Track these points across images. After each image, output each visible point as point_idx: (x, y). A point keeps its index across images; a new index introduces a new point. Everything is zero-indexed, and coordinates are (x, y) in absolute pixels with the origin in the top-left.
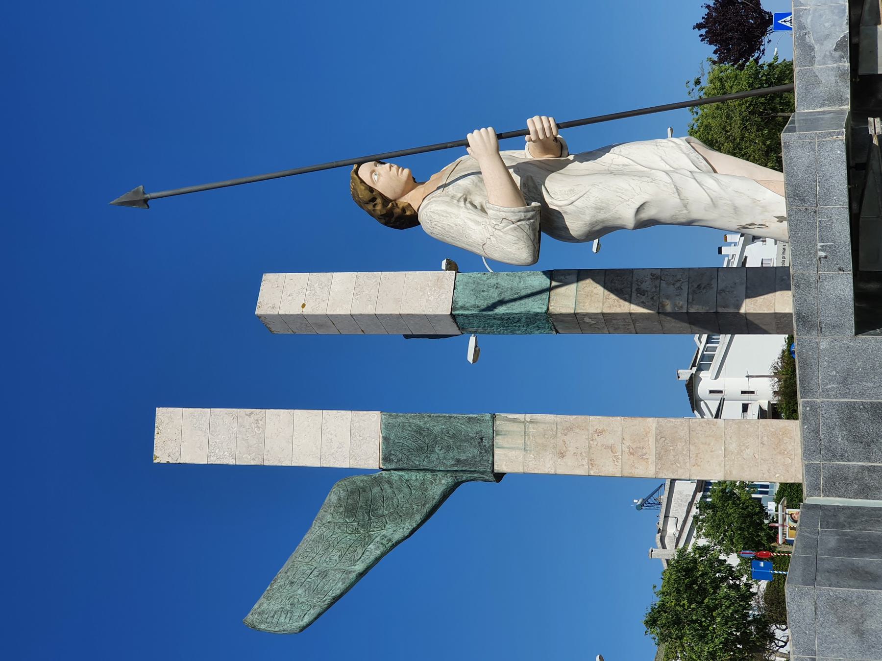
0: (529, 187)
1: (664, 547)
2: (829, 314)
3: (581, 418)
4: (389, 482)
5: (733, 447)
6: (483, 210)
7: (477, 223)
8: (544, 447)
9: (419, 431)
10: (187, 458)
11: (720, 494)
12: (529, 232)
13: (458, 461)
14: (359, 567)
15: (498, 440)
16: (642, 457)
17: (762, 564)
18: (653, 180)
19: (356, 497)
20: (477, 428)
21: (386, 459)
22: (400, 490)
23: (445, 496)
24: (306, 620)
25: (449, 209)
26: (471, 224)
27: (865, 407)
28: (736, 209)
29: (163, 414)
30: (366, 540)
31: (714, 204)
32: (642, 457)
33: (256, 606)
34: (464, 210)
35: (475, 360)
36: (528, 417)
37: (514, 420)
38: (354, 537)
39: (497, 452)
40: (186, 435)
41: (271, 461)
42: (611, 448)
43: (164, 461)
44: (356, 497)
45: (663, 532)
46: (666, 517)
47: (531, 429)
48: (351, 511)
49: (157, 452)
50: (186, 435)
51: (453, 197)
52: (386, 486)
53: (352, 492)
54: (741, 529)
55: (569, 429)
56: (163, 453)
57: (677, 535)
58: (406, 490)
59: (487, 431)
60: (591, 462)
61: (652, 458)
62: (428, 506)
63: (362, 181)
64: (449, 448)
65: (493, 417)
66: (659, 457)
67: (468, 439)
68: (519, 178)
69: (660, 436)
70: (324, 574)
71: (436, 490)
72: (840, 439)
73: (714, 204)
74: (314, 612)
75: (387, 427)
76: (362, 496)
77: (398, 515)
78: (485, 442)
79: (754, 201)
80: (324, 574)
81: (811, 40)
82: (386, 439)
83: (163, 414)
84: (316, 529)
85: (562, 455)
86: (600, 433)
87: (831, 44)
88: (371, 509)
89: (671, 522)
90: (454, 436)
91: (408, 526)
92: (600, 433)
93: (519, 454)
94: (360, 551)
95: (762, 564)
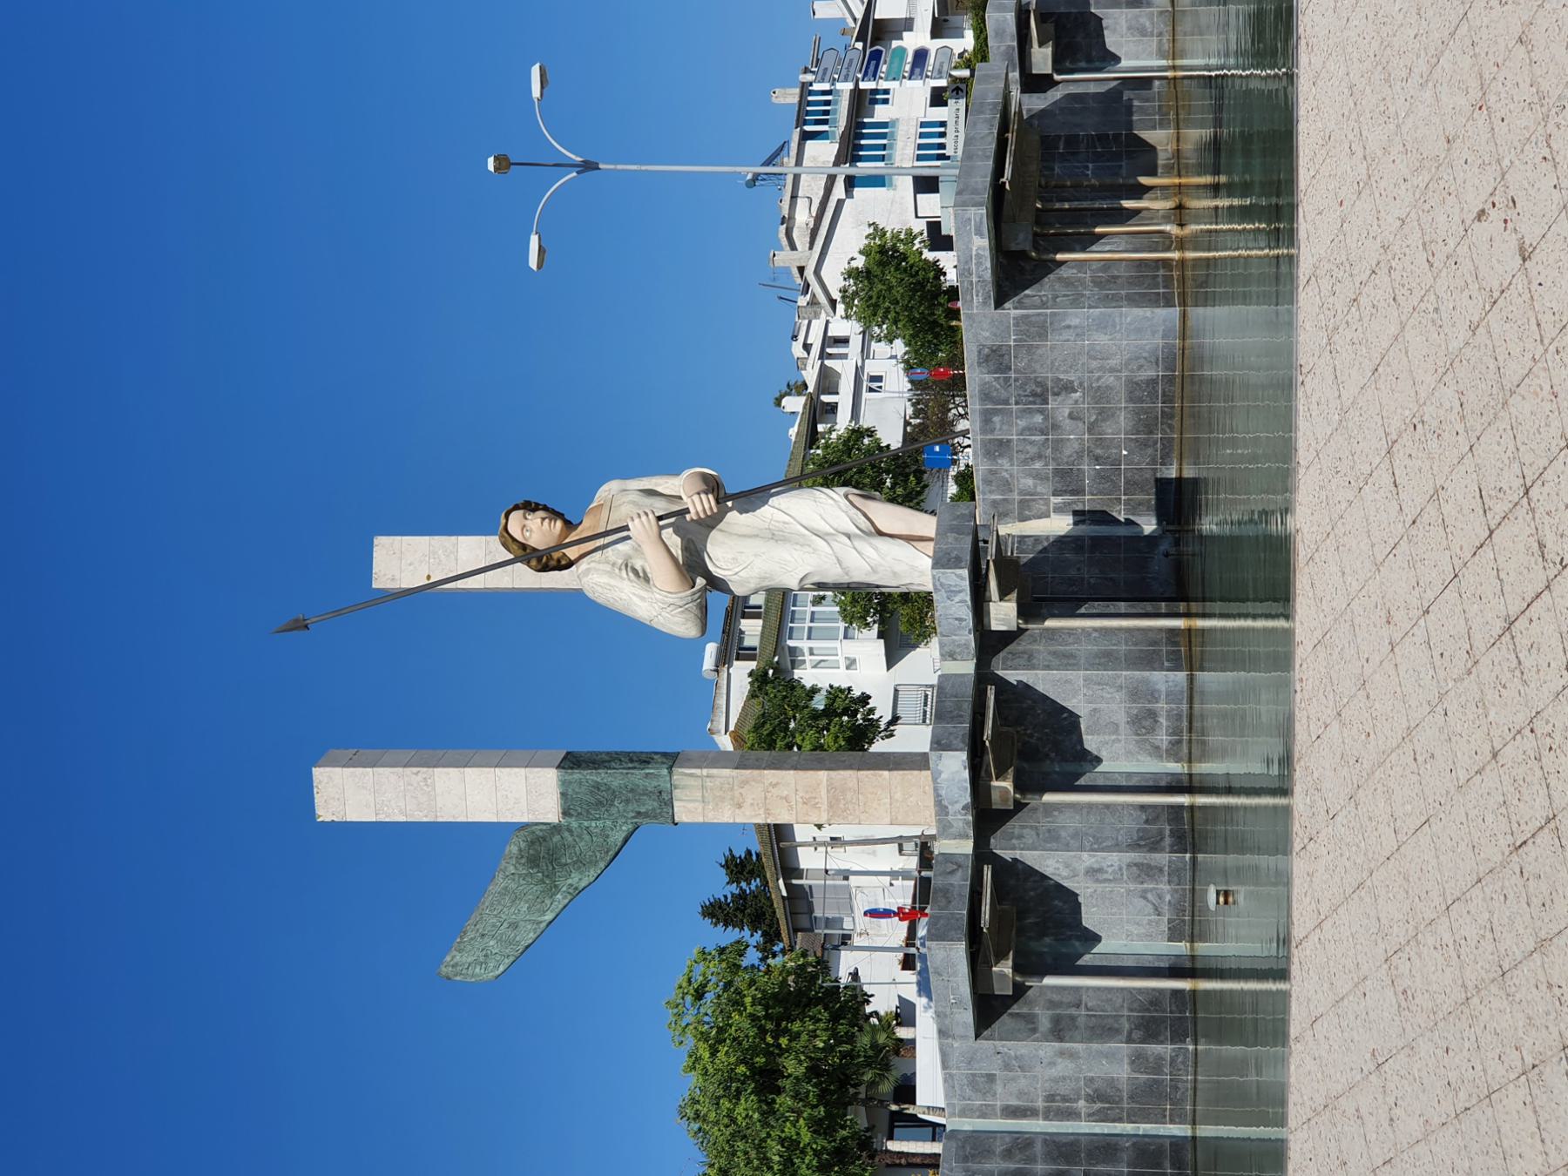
0: (693, 565)
1: (793, 247)
2: (959, 1031)
3: (756, 772)
4: (570, 830)
5: (898, 796)
6: (647, 579)
7: (643, 599)
8: (722, 799)
9: (597, 786)
10: (353, 817)
11: (878, 257)
12: (697, 612)
13: (639, 813)
14: (549, 917)
15: (676, 793)
16: (815, 806)
17: (937, 448)
18: (815, 550)
19: (537, 846)
20: (655, 783)
21: (565, 813)
22: (579, 836)
23: (626, 841)
24: (502, 969)
25: (612, 582)
26: (635, 599)
27: (982, 1075)
28: (895, 574)
29: (320, 774)
30: (553, 889)
31: (874, 571)
32: (815, 806)
33: (448, 958)
34: (626, 582)
35: (540, 266)
36: (705, 772)
37: (691, 775)
38: (539, 888)
39: (676, 804)
40: (349, 793)
41: (444, 817)
42: (786, 798)
43: (328, 819)
44: (537, 846)
45: (788, 221)
46: (794, 197)
47: (709, 784)
48: (533, 862)
49: (319, 811)
50: (349, 793)
51: (614, 565)
52: (566, 834)
53: (533, 843)
54: (906, 308)
55: (745, 783)
56: (326, 811)
57: (811, 225)
58: (587, 837)
59: (666, 786)
60: (768, 812)
61: (825, 807)
62: (611, 853)
63: (514, 540)
64: (628, 801)
65: (670, 773)
66: (831, 806)
67: (646, 793)
68: (678, 540)
69: (831, 787)
70: (514, 926)
71: (618, 837)
72: (968, 1092)
73: (874, 571)
74: (507, 961)
75: (564, 783)
76: (542, 850)
77: (581, 863)
78: (664, 795)
79: (912, 567)
80: (514, 926)
81: (945, 803)
82: (562, 794)
83: (320, 774)
84: (500, 882)
85: (740, 807)
86: (774, 785)
87: (959, 806)
88: (553, 857)
89: (801, 204)
90: (632, 790)
91: (593, 873)
92: (774, 785)
93: (699, 806)
94: (548, 902)
95: (937, 448)
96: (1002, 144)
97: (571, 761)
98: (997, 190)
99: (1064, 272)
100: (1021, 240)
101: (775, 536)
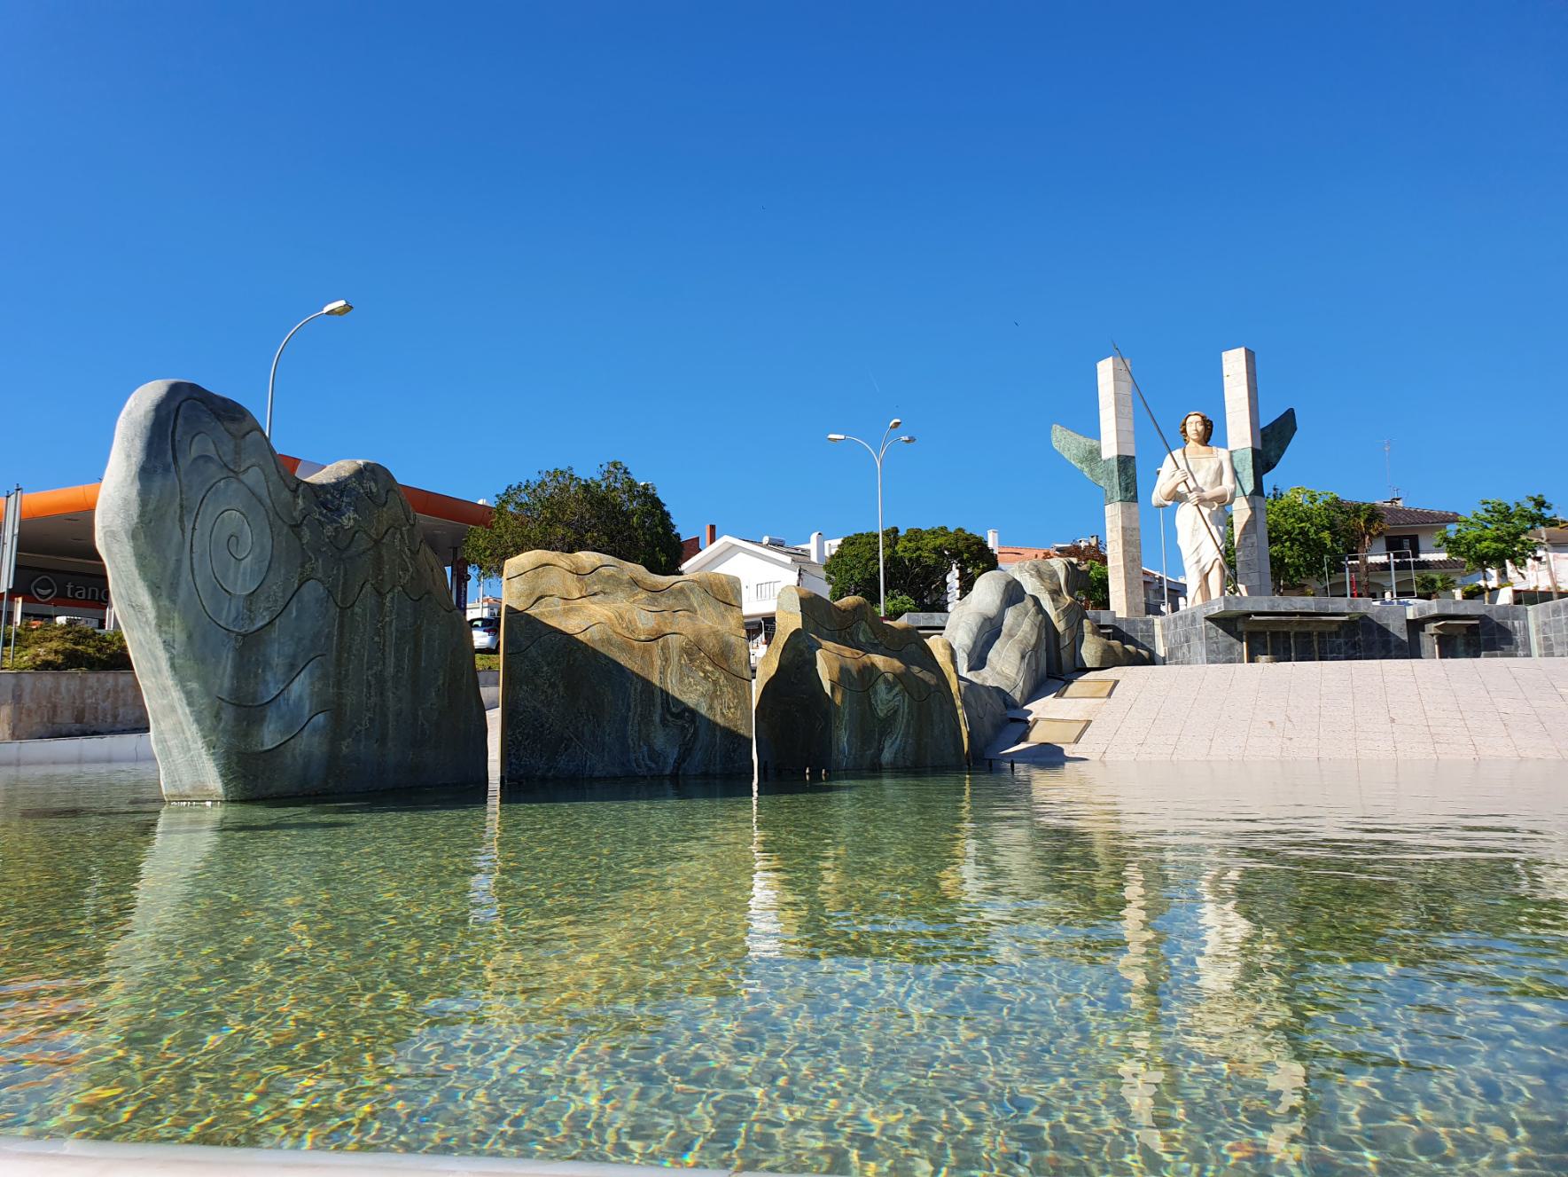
0: (1177, 498)
48: (1091, 452)
76: (1094, 455)
84: (1082, 439)
96: (1302, 614)
97: (1125, 462)
98: (1249, 615)
99: (1238, 647)
100: (1241, 627)
101: (1195, 531)
